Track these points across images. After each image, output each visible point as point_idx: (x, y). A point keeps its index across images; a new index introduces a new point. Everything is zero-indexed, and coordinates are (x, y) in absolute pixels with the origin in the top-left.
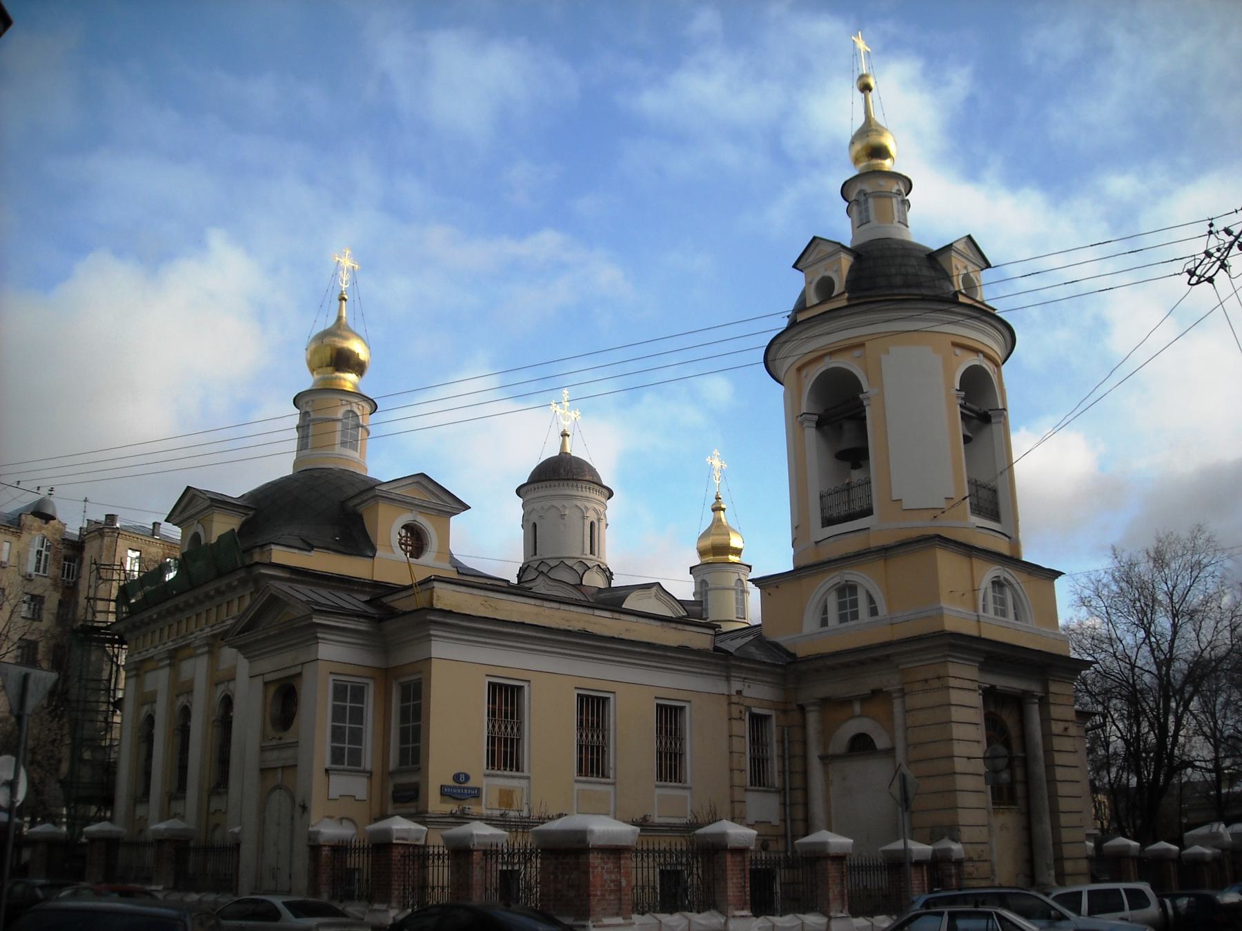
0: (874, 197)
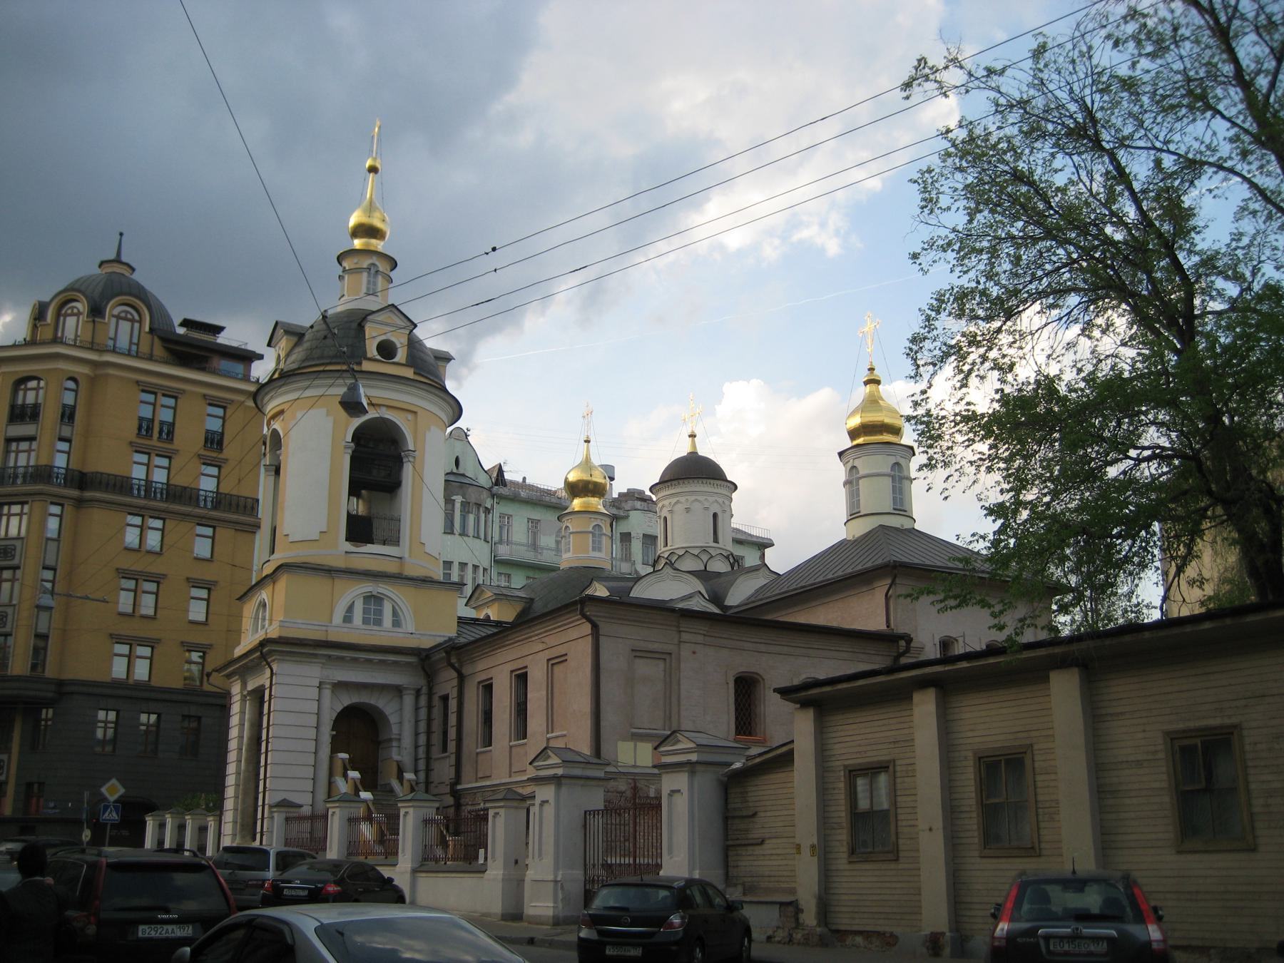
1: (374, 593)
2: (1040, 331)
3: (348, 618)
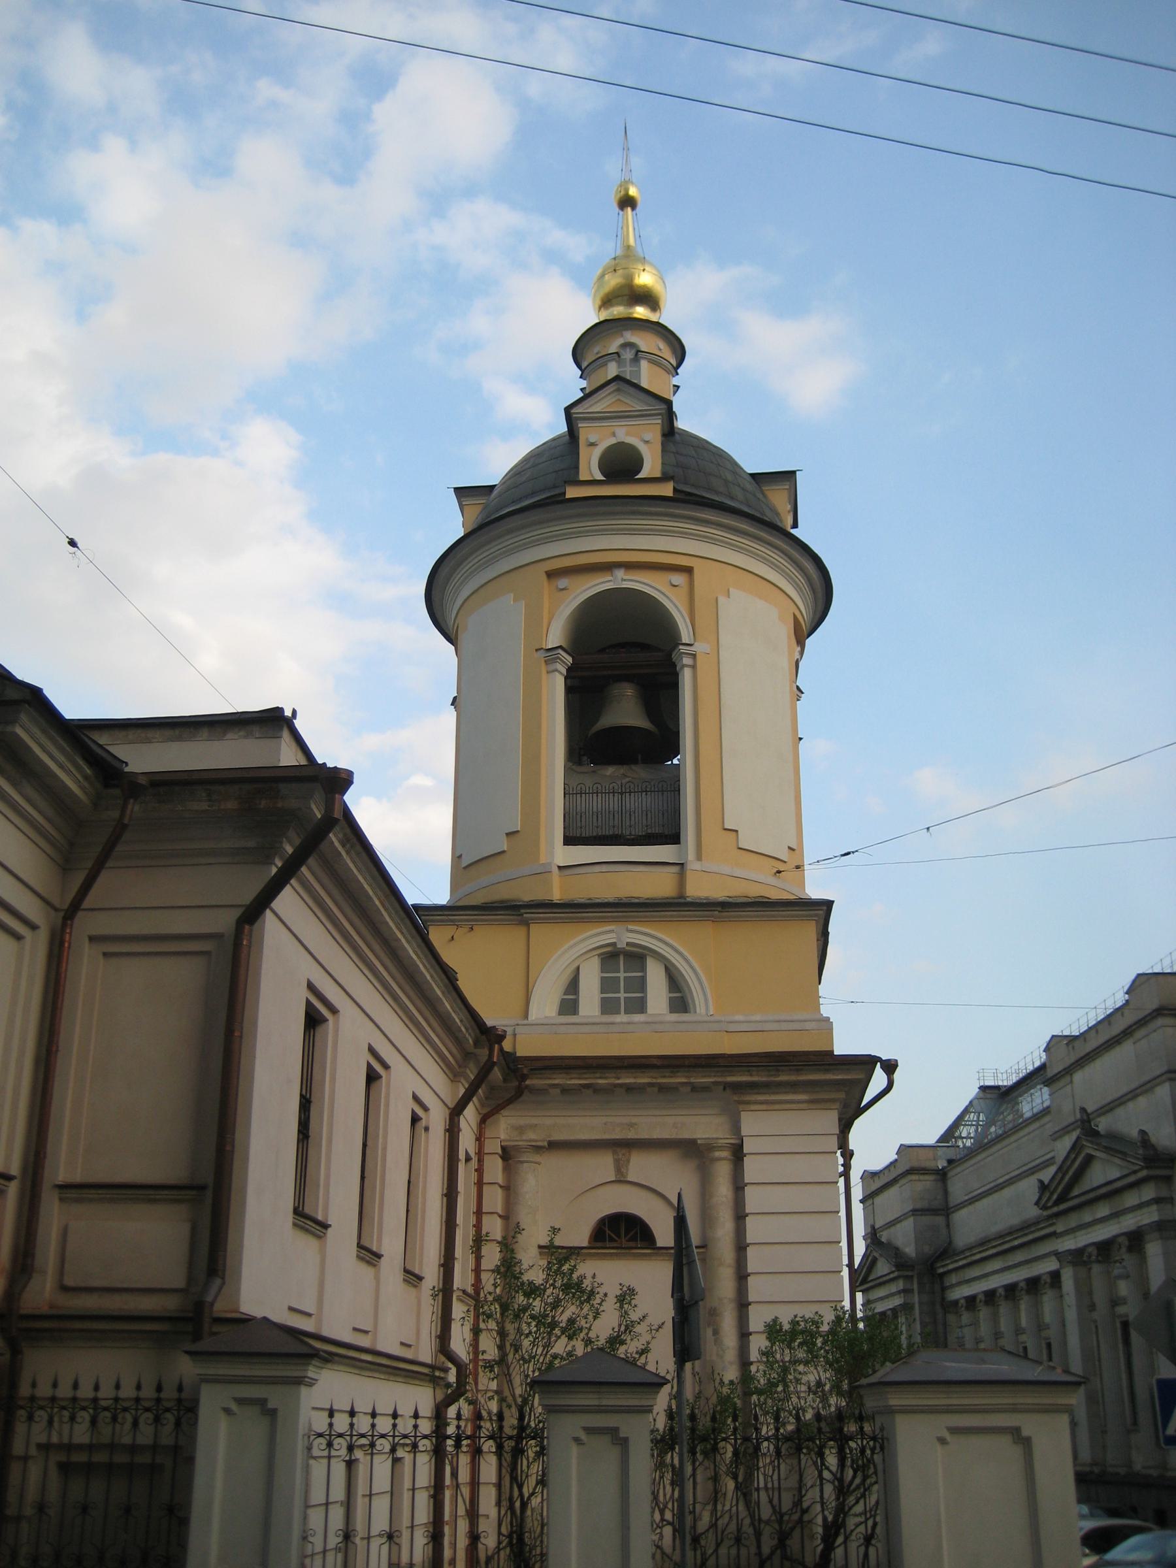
0: (651, 361)
1: (621, 945)
2: (719, 1541)
3: (569, 1006)
